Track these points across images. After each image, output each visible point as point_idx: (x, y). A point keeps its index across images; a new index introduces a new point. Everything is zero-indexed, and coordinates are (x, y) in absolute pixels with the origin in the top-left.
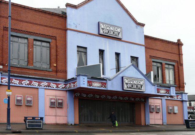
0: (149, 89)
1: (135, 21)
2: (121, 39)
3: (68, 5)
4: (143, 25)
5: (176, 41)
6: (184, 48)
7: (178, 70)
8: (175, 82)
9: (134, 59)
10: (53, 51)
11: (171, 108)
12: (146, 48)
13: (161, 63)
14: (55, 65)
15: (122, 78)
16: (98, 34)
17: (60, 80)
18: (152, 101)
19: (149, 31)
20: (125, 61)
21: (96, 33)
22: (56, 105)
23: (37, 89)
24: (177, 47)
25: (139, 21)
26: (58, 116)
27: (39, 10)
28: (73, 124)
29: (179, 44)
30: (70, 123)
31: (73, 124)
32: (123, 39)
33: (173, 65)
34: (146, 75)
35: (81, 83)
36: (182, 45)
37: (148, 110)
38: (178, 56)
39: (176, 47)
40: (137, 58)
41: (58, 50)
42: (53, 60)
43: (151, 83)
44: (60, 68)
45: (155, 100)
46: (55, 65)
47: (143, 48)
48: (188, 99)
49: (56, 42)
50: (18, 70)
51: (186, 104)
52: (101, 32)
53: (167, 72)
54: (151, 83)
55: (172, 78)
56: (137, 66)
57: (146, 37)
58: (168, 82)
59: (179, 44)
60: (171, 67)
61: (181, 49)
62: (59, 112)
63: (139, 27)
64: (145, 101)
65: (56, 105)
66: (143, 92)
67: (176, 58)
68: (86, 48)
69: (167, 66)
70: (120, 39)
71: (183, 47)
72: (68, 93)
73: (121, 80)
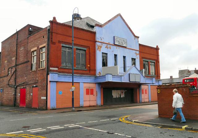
0: (143, 80)
1: (134, 35)
4: (138, 37)
5: (156, 47)
6: (160, 51)
7: (157, 66)
8: (155, 73)
9: (134, 59)
10: (88, 56)
12: (140, 52)
13: (147, 61)
14: (89, 66)
15: (129, 74)
16: (113, 44)
17: (176, 84)
18: (143, 87)
19: (141, 42)
20: (129, 62)
21: (112, 43)
22: (89, 92)
23: (78, 83)
24: (156, 51)
28: (100, 105)
29: (157, 49)
30: (98, 105)
31: (100, 105)
32: (127, 47)
33: (154, 63)
34: (140, 71)
35: (109, 78)
37: (141, 92)
38: (156, 56)
39: (155, 51)
40: (135, 59)
41: (91, 55)
42: (88, 63)
43: (143, 76)
44: (91, 68)
45: (145, 86)
46: (89, 66)
47: (138, 52)
49: (90, 50)
50: (67, 71)
52: (117, 43)
53: (151, 66)
54: (143, 76)
55: (153, 71)
56: (134, 64)
57: (140, 45)
58: (151, 74)
60: (153, 63)
61: (159, 52)
62: (91, 97)
63: (136, 39)
64: (139, 87)
65: (89, 92)
67: (156, 59)
68: (107, 54)
69: (151, 63)
70: (125, 47)
71: (159, 50)
72: (97, 84)
73: (129, 75)
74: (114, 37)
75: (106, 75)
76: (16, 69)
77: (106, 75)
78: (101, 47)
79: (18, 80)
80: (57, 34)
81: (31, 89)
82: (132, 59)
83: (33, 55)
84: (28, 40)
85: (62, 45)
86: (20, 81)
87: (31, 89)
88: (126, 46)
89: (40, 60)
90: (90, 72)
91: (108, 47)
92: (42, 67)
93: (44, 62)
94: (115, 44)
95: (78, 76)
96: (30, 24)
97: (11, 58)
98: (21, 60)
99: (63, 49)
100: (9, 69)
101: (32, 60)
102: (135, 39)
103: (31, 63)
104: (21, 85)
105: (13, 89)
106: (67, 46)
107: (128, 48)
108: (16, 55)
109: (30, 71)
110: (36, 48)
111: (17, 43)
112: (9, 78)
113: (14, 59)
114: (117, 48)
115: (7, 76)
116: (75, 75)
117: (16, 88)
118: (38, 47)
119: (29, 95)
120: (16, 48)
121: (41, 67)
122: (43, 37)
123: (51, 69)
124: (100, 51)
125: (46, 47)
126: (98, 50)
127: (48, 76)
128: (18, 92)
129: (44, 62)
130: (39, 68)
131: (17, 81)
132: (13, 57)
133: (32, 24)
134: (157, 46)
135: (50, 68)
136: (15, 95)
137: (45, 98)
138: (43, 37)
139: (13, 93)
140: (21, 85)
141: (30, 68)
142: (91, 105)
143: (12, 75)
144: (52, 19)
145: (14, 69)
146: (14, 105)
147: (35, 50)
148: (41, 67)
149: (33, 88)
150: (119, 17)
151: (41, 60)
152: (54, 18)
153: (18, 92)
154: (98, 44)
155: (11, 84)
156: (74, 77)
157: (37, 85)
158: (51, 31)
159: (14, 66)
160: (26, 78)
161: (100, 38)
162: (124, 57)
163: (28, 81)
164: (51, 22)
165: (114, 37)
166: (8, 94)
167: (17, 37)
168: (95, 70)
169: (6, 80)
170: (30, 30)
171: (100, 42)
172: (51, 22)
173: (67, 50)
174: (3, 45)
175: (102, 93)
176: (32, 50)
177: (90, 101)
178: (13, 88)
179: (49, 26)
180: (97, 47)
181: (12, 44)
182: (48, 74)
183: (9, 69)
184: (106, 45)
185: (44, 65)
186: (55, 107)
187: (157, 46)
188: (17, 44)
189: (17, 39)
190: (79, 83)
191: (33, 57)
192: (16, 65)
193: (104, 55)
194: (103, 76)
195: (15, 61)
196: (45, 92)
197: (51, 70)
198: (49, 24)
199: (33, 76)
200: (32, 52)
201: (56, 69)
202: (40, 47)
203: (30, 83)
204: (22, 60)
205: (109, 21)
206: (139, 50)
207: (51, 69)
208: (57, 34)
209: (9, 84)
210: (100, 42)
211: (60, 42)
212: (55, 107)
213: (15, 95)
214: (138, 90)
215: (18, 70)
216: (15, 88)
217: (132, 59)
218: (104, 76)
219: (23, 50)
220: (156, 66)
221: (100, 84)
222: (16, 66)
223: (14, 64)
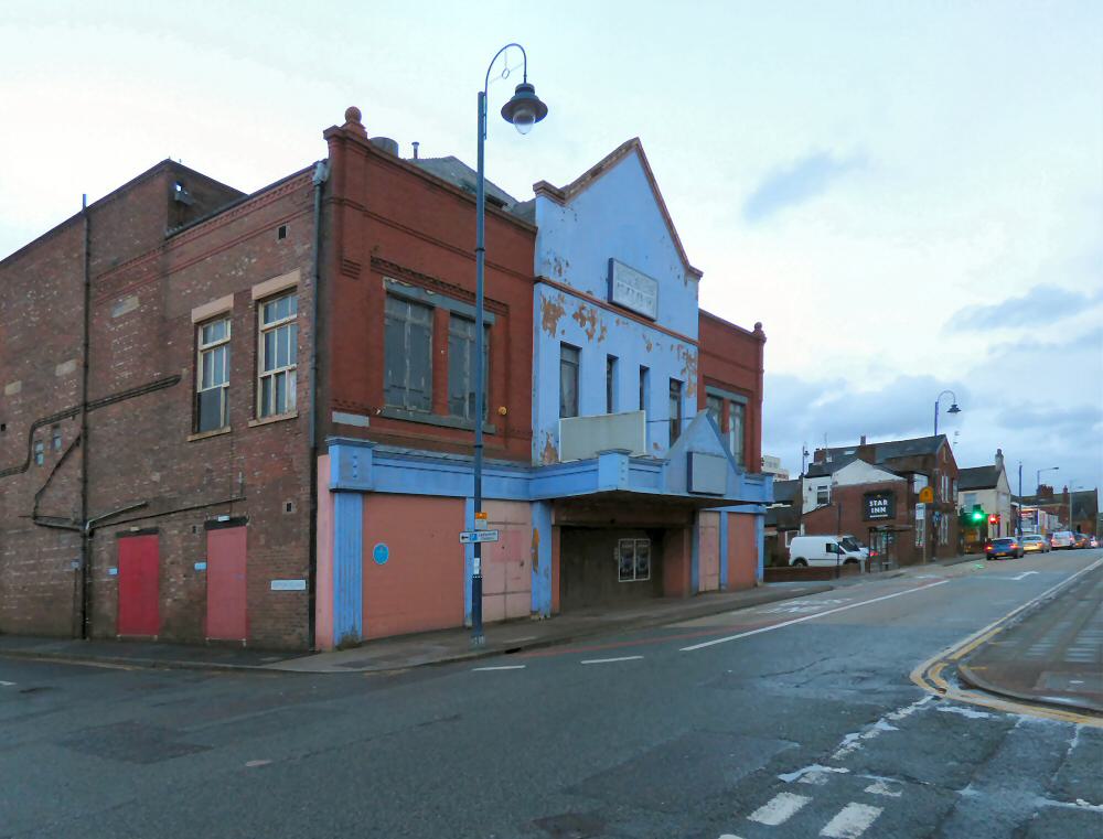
1: (685, 262)
2: (652, 320)
3: (543, 188)
5: (751, 329)
9: (676, 385)
11: (993, 519)
13: (720, 399)
14: (503, 410)
16: (605, 302)
18: (708, 521)
21: (600, 295)
25: (693, 263)
26: (509, 593)
27: (382, 155)
29: (757, 339)
33: (742, 405)
36: (1051, 489)
45: (708, 514)
46: (503, 410)
47: (693, 350)
48: (775, 494)
50: (410, 434)
51: (463, 512)
59: (347, 138)
66: (720, 495)
72: (538, 507)
73: (685, 461)
74: (611, 262)
75: (602, 459)
76: (85, 428)
77: (602, 459)
78: (558, 312)
79: (98, 490)
80: (368, 214)
81: (197, 535)
82: (672, 380)
83: (205, 342)
84: (166, 252)
85: (388, 283)
86: (113, 493)
87: (197, 535)
88: (653, 316)
89: (255, 373)
90: (506, 447)
91: (585, 313)
92: (272, 409)
93: (290, 383)
94: (615, 299)
95: (457, 463)
96: (175, 159)
97: (50, 363)
98: (122, 371)
99: (392, 309)
100: (34, 428)
101: (195, 369)
102: (686, 283)
103: (195, 387)
104: (122, 518)
105: (71, 542)
106: (412, 292)
107: (664, 326)
108: (86, 345)
109: (189, 439)
110: (226, 302)
111: (88, 278)
112: (35, 479)
113: (67, 368)
114: (618, 322)
115: (26, 467)
116: (493, 461)
117: (92, 534)
118: (242, 297)
119: (180, 572)
120: (81, 308)
121: (265, 413)
122: (282, 233)
123: (340, 418)
124: (553, 331)
125: (307, 292)
126: (545, 329)
127: (320, 459)
128: (105, 555)
129: (290, 383)
130: (255, 417)
131: (92, 495)
132: (64, 361)
133: (186, 163)
134: (758, 326)
135: (334, 414)
136: (86, 572)
137: (300, 585)
138: (282, 233)
139: (76, 565)
140: (122, 518)
141: (188, 419)
142: (511, 614)
143: (59, 465)
144: (341, 121)
145: (71, 429)
146: (79, 630)
147: (223, 315)
148: (264, 414)
149: (212, 533)
150: (633, 156)
151: (262, 373)
152: (353, 115)
153: (105, 555)
154: (543, 293)
155: (50, 513)
156: (483, 472)
157: (233, 515)
158: (333, 191)
159: (72, 413)
160: (156, 477)
161: (554, 264)
162: (644, 371)
163: (175, 495)
164: (333, 135)
165: (611, 262)
166: (34, 567)
167: (89, 242)
168: (528, 434)
169: (18, 492)
170: (177, 197)
171: (555, 286)
172: (333, 135)
173: (409, 313)
174: (115, 197)
175: (558, 550)
176: (198, 314)
177: (504, 593)
178: (72, 534)
179: (325, 162)
180: (539, 315)
181: (55, 287)
182: (317, 450)
183: (34, 428)
184: (577, 302)
185: (291, 396)
186: (360, 633)
187: (758, 326)
188: (88, 285)
189: (88, 254)
190: (464, 498)
191: (206, 353)
192: (86, 406)
193: (569, 356)
194: (581, 463)
195: (76, 383)
196: (302, 553)
197: (337, 429)
198: (322, 151)
199: (207, 465)
200: (200, 323)
201: (361, 421)
202: (258, 291)
203: (187, 504)
204: (126, 374)
205: (596, 172)
206: (696, 338)
207: (340, 418)
208: (368, 214)
209: (40, 512)
210: (555, 286)
211: (381, 267)
212: (360, 633)
213: (86, 572)
214: (686, 533)
215: (97, 431)
216: (84, 537)
217: (672, 380)
218: (586, 465)
219: (129, 316)
220: (749, 421)
221: (551, 503)
222: (86, 411)
223: (70, 399)
